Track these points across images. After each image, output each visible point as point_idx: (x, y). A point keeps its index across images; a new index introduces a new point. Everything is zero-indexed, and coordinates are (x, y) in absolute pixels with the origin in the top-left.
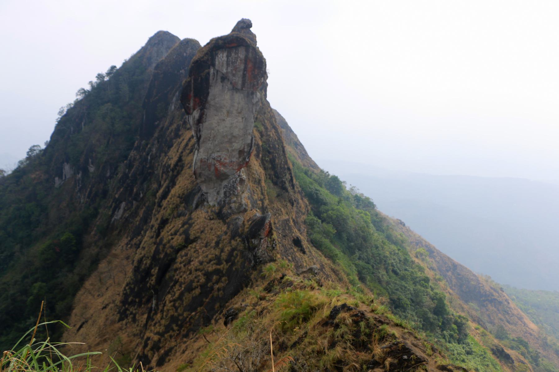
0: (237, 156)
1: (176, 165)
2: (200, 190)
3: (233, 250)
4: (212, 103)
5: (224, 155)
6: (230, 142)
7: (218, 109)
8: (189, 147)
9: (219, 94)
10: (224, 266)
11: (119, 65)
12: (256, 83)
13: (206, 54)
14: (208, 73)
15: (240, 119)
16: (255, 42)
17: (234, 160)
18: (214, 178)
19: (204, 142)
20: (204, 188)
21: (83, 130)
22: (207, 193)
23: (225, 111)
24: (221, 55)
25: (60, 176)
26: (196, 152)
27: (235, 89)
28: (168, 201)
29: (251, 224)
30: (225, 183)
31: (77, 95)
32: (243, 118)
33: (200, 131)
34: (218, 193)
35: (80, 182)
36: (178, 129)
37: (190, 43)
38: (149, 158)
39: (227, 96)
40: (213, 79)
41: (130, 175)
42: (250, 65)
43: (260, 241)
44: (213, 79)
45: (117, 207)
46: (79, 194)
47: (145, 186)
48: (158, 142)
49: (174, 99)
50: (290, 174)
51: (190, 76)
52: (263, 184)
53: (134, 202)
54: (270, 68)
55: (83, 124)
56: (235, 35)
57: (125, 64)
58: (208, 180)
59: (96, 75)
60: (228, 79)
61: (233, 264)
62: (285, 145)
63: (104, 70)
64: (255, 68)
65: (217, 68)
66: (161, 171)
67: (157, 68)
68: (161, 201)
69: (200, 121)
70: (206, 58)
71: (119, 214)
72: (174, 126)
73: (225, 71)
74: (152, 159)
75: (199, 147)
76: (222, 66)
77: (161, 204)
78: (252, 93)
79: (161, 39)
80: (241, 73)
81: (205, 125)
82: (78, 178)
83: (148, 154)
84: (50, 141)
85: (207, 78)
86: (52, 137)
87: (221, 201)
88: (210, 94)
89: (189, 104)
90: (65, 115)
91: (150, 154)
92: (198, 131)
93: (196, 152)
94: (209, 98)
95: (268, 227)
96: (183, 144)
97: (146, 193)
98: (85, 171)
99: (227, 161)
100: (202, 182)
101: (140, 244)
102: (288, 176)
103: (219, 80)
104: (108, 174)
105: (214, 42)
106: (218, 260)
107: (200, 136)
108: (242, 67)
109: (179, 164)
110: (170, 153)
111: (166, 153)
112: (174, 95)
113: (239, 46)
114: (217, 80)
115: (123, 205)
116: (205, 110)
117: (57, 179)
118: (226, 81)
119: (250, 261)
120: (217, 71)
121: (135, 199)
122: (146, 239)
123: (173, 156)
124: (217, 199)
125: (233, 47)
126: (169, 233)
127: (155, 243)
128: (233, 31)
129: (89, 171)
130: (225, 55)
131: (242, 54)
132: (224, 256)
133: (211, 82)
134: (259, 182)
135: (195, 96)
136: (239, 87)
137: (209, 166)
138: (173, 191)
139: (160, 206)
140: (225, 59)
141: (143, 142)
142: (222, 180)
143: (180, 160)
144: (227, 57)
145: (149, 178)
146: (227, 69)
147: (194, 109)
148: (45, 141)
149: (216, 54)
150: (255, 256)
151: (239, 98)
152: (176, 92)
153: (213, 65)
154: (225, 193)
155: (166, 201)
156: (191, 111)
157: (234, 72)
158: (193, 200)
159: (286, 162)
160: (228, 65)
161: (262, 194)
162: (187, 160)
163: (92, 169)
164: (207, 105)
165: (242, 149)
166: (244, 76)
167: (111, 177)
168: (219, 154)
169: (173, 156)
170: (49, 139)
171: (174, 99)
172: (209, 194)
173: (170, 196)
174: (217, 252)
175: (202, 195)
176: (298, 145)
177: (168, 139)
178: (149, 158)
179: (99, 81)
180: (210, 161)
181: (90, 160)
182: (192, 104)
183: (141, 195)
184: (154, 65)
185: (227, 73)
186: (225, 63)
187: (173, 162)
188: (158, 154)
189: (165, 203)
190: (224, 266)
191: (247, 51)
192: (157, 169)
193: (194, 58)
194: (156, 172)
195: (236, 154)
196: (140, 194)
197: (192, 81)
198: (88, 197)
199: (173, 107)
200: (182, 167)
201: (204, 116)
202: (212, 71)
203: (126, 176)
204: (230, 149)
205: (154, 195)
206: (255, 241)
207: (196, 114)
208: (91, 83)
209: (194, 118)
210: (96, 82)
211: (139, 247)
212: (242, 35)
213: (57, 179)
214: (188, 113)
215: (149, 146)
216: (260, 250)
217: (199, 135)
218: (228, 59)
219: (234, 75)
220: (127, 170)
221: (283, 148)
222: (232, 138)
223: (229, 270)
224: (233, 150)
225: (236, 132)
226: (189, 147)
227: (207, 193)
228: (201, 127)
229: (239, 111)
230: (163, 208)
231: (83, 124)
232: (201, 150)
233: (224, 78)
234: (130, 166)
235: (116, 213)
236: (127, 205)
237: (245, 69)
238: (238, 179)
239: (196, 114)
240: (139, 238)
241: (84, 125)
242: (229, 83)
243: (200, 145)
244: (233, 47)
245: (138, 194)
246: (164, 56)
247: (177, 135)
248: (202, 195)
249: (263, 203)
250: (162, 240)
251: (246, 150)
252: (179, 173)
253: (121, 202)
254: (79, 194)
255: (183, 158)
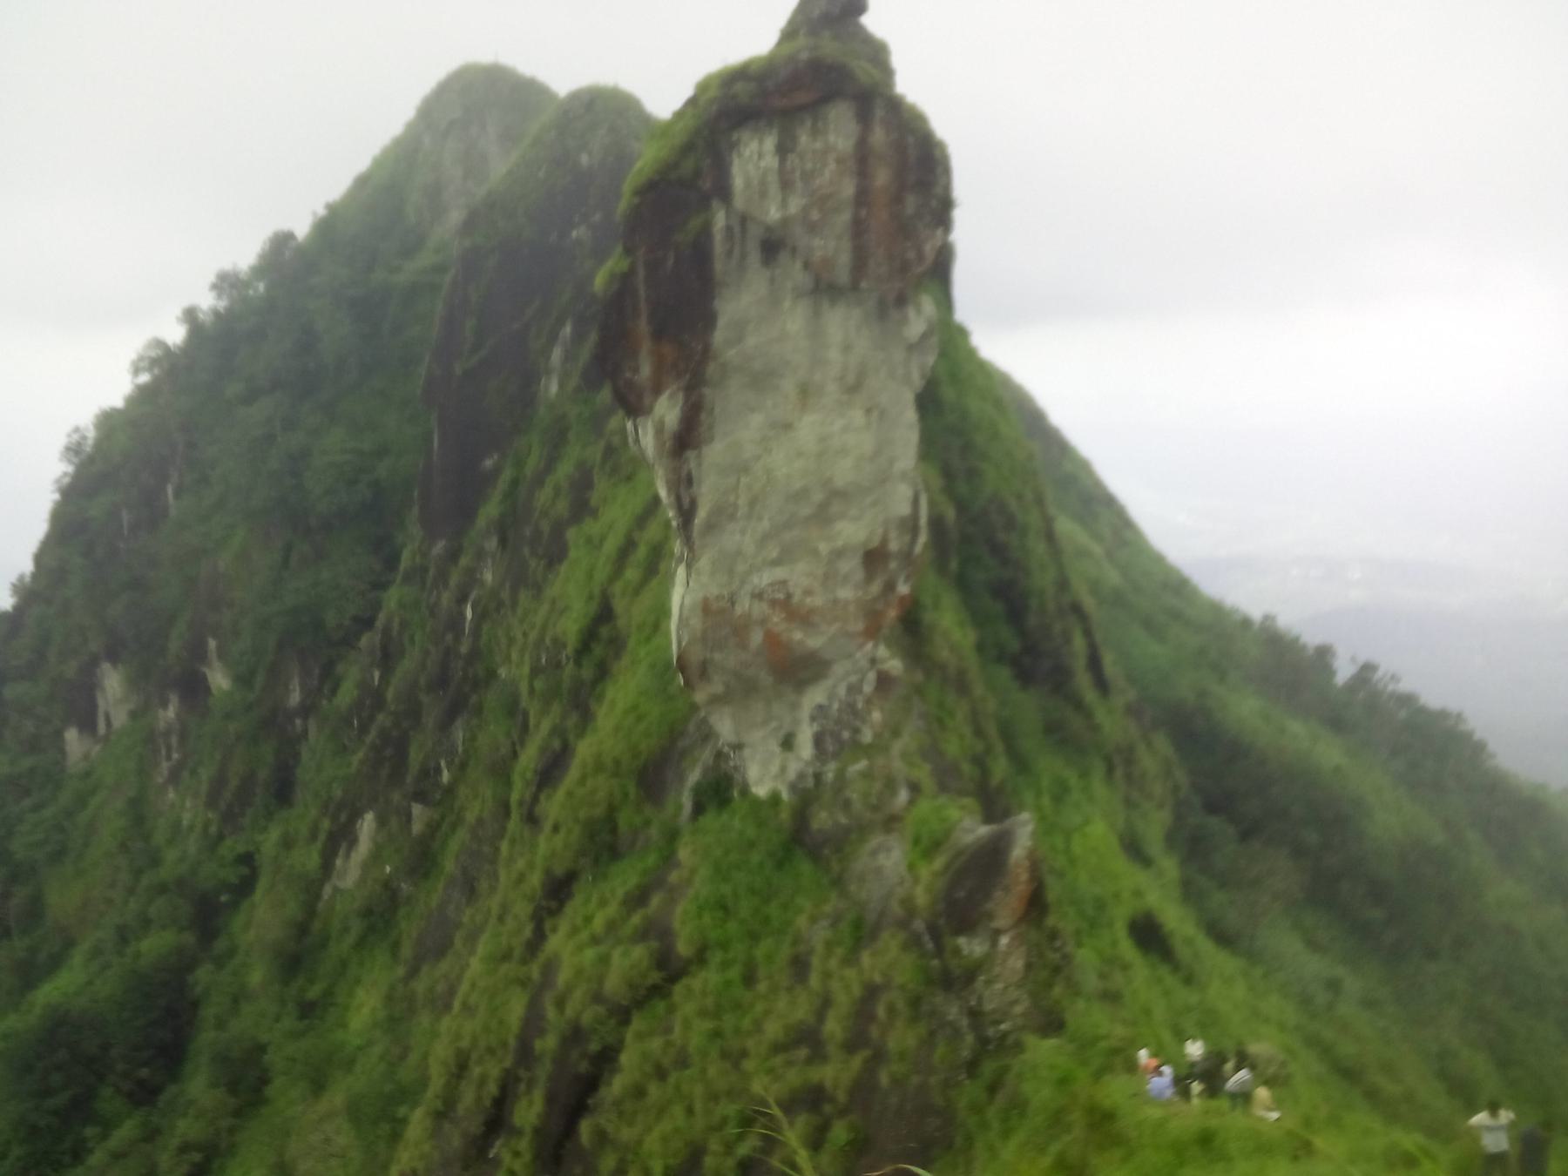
0: (859, 575)
1: (589, 637)
2: (708, 735)
3: (872, 992)
4: (731, 354)
5: (799, 576)
6: (823, 517)
7: (762, 379)
8: (641, 552)
9: (758, 317)
10: (836, 1073)
11: (302, 229)
12: (911, 255)
13: (688, 148)
14: (706, 231)
15: (858, 416)
16: (887, 72)
17: (846, 593)
18: (766, 679)
19: (711, 527)
20: (724, 726)
21: (173, 512)
22: (738, 747)
23: (789, 386)
24: (754, 145)
25: (87, 724)
26: (681, 572)
27: (823, 289)
28: (570, 794)
29: (947, 867)
30: (815, 696)
31: (136, 371)
32: (868, 411)
33: (689, 481)
34: (788, 743)
35: (174, 740)
36: (582, 484)
37: (604, 110)
38: (469, 614)
39: (795, 320)
40: (729, 253)
41: (390, 694)
42: (882, 177)
43: (994, 943)
44: (729, 253)
45: (342, 837)
46: (171, 795)
47: (459, 734)
48: (503, 542)
49: (557, 354)
50: (1088, 633)
51: (628, 251)
52: (979, 690)
53: (417, 809)
54: (964, 184)
55: (170, 490)
56: (804, 56)
57: (329, 226)
58: (742, 691)
59: (212, 278)
60: (794, 250)
61: (879, 1057)
62: (1052, 510)
63: (244, 254)
64: (905, 186)
65: (739, 202)
66: (526, 670)
67: (469, 226)
68: (535, 799)
69: (686, 439)
70: (688, 166)
71: (351, 871)
72: (565, 469)
73: (774, 214)
74: (481, 617)
75: (691, 549)
76: (763, 194)
77: (538, 810)
78: (901, 301)
79: (480, 99)
80: (845, 217)
81: (714, 453)
82: (162, 725)
83: (462, 600)
84: (35, 576)
85: (700, 253)
86: (39, 558)
87: (801, 776)
88: (722, 322)
89: (636, 370)
90: (91, 460)
91: (473, 596)
92: (683, 483)
93: (681, 572)
94: (719, 336)
95: (1024, 877)
96: (611, 545)
97: (463, 766)
98: (193, 688)
99: (817, 601)
100: (716, 700)
101: (452, 992)
102: (1079, 643)
103: (754, 257)
104: (295, 698)
105: (713, 93)
106: (807, 1039)
107: (693, 504)
108: (848, 189)
109: (604, 631)
110: (553, 591)
111: (538, 589)
112: (553, 338)
113: (827, 98)
114: (743, 256)
115: (367, 825)
116: (707, 391)
117: (71, 735)
118: (784, 257)
119: (957, 1033)
120: (744, 220)
121: (420, 796)
122: (476, 965)
123: (566, 600)
124: (783, 769)
125: (802, 108)
126: (584, 936)
127: (523, 983)
128: (789, 34)
129: (207, 690)
130: (770, 143)
131: (839, 130)
132: (834, 1027)
133: (719, 266)
134: (962, 687)
135: (658, 335)
136: (843, 275)
137: (740, 630)
138: (584, 750)
139: (532, 819)
140: (771, 161)
141: (439, 547)
142: (801, 685)
143: (605, 614)
144: (783, 150)
145: (474, 699)
146: (784, 204)
147: (657, 390)
148: (13, 578)
149: (733, 146)
150: (975, 1014)
151: (843, 325)
152: (560, 322)
153: (723, 191)
154: (818, 741)
155: (560, 794)
156: (647, 401)
157: (815, 215)
158: (681, 778)
159: (1063, 584)
160: (786, 185)
161: (979, 732)
162: (631, 613)
163: (219, 680)
164: (711, 369)
165: (875, 543)
166: (858, 229)
167: (306, 710)
168: (780, 573)
169: (566, 600)
170: (27, 566)
171: (557, 354)
172: (747, 752)
173: (573, 773)
174: (802, 1011)
175: (719, 755)
176: (1096, 504)
177: (545, 527)
178: (469, 614)
179: (222, 304)
180: (744, 605)
181: (212, 644)
182: (646, 371)
183: (446, 776)
184: (455, 217)
185: (785, 222)
186: (773, 179)
187: (570, 627)
188: (505, 595)
189: (553, 806)
190: (836, 1073)
191: (864, 117)
192: (508, 658)
193: (639, 165)
194: (503, 672)
195: (851, 566)
196: (438, 771)
197: (641, 273)
198: (211, 802)
199: (554, 388)
200: (617, 645)
201: (703, 416)
202: (720, 220)
203: (372, 699)
204: (824, 548)
205: (501, 771)
206: (972, 947)
207: (668, 409)
208: (190, 315)
209: (660, 430)
210: (216, 313)
211: (448, 1007)
212: (830, 48)
213: (71, 735)
214: (633, 406)
215: (464, 561)
216: (999, 986)
217: (686, 502)
218: (782, 161)
219: (813, 228)
220: (377, 674)
221: (1048, 522)
222: (831, 502)
223: (863, 1089)
224: (838, 554)
225: (843, 472)
226: (641, 552)
227: (738, 747)
228: (692, 465)
229: (851, 379)
230: (547, 826)
231: (170, 490)
232: (704, 563)
233: (772, 247)
234: (387, 657)
235: (339, 862)
236: (382, 821)
237: (862, 198)
238: (872, 676)
239: (668, 409)
240: (445, 966)
241: (177, 495)
242: (798, 265)
243: (697, 543)
244: (802, 108)
245: (429, 772)
246: (500, 166)
247: (582, 508)
248: (719, 755)
249: (985, 772)
250: (550, 969)
251: (894, 546)
252: (603, 672)
253: (356, 815)
254: (171, 795)
255: (619, 605)
